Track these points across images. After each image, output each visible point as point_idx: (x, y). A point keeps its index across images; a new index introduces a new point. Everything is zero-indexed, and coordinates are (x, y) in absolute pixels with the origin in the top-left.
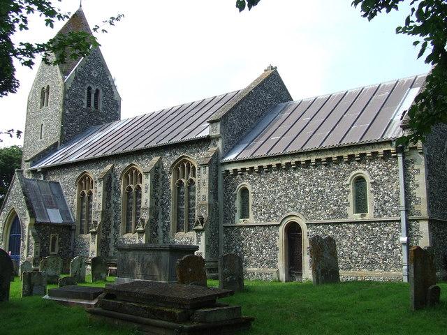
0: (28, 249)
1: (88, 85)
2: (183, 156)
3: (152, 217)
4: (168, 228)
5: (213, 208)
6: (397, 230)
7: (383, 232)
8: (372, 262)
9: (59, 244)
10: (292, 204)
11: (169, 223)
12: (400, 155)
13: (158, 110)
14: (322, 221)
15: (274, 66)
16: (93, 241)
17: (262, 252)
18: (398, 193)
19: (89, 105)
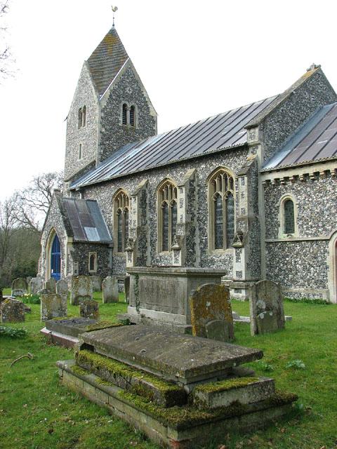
1: (123, 102)
4: (206, 246)
9: (98, 262)
13: (193, 122)
15: (317, 64)
19: (125, 122)
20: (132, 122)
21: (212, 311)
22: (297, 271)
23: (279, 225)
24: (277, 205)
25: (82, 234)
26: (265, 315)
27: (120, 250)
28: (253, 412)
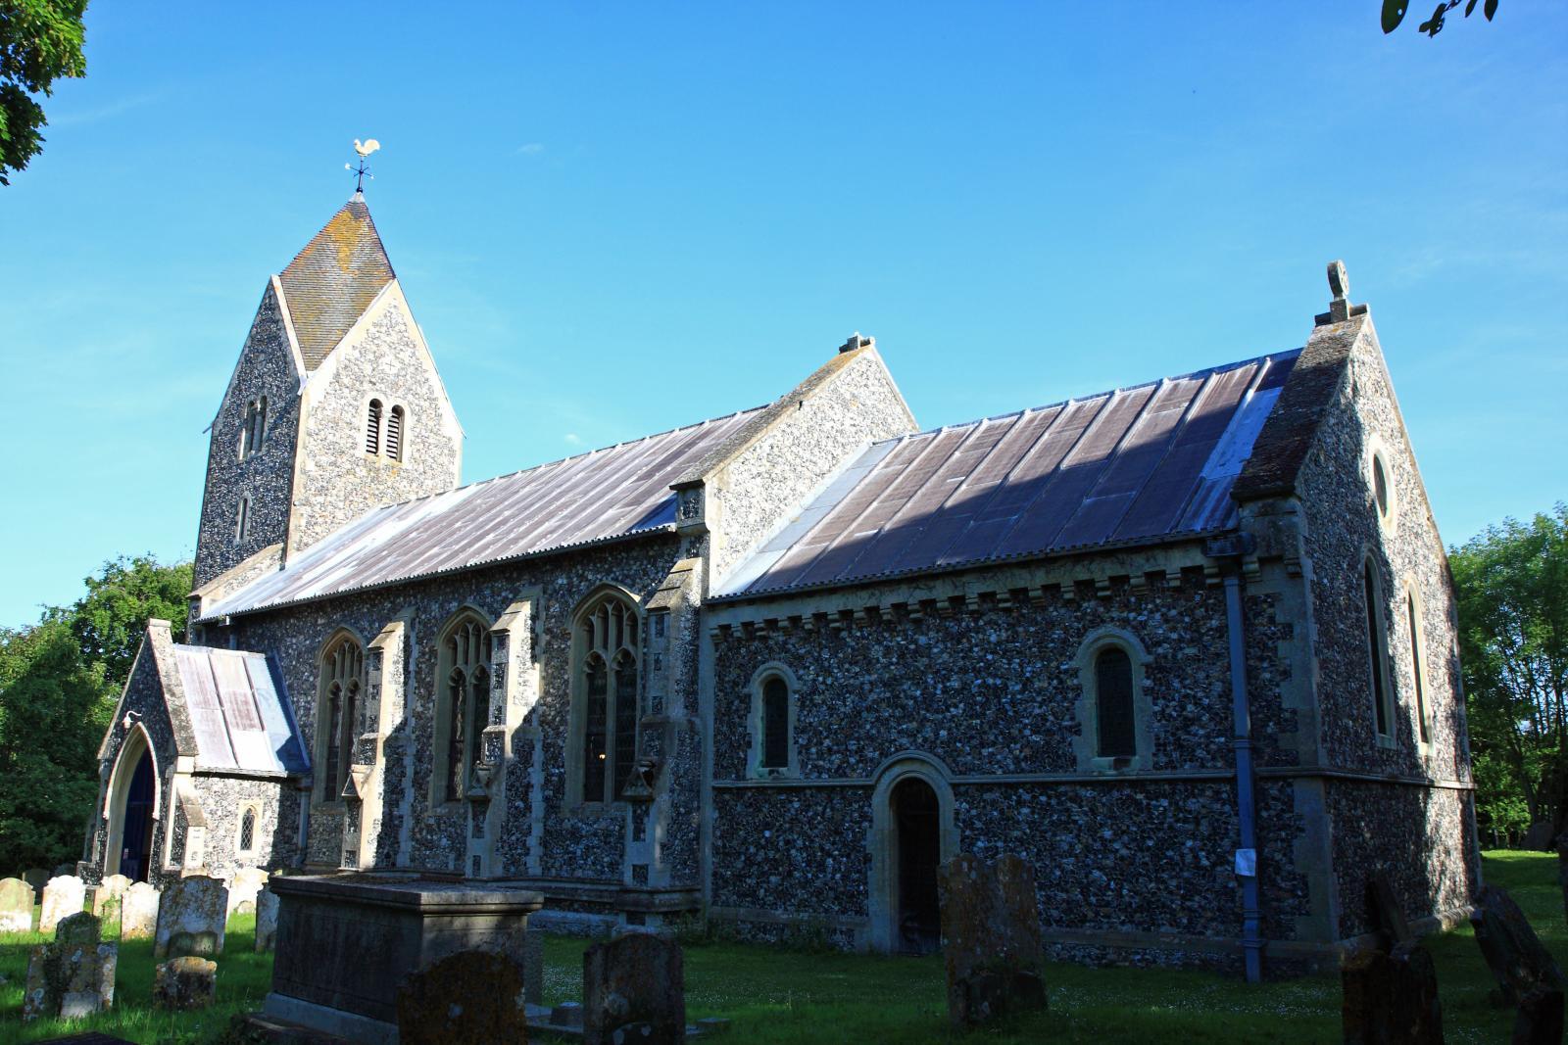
4: (559, 789)
6: (1227, 808)
11: (561, 776)
17: (822, 867)
22: (793, 866)
23: (749, 745)
24: (746, 690)
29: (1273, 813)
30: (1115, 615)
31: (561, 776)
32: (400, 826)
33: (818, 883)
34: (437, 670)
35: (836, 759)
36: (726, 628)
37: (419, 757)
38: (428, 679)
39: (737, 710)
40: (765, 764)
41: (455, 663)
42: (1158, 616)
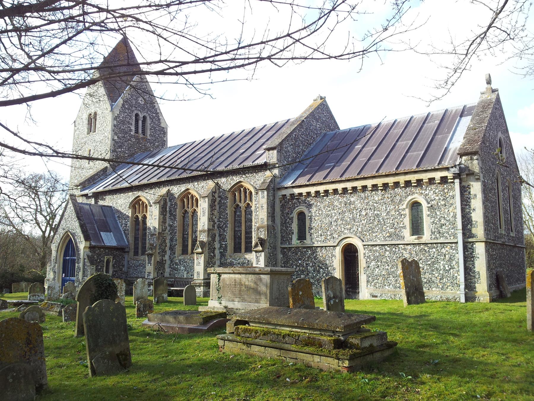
0: (84, 272)
1: (136, 112)
2: (240, 182)
3: (210, 239)
4: (225, 249)
5: (270, 229)
6: (454, 251)
7: (440, 254)
8: (429, 281)
9: (113, 266)
10: (348, 227)
11: (226, 245)
12: (457, 181)
13: (208, 137)
14: (379, 242)
15: (323, 96)
16: (149, 262)
17: (319, 272)
18: (455, 216)
19: (137, 131)
20: (144, 132)
21: (302, 298)
22: (309, 272)
23: (293, 233)
24: (291, 216)
25: (99, 239)
26: (335, 302)
27: (136, 253)
28: (379, 351)
29: (469, 253)
30: (418, 191)
31: (226, 245)
32: (165, 263)
33: (318, 277)
34: (178, 210)
35: (323, 237)
36: (284, 196)
37: (171, 240)
38: (174, 213)
39: (288, 222)
40: (298, 239)
41: (184, 208)
42: (432, 192)
